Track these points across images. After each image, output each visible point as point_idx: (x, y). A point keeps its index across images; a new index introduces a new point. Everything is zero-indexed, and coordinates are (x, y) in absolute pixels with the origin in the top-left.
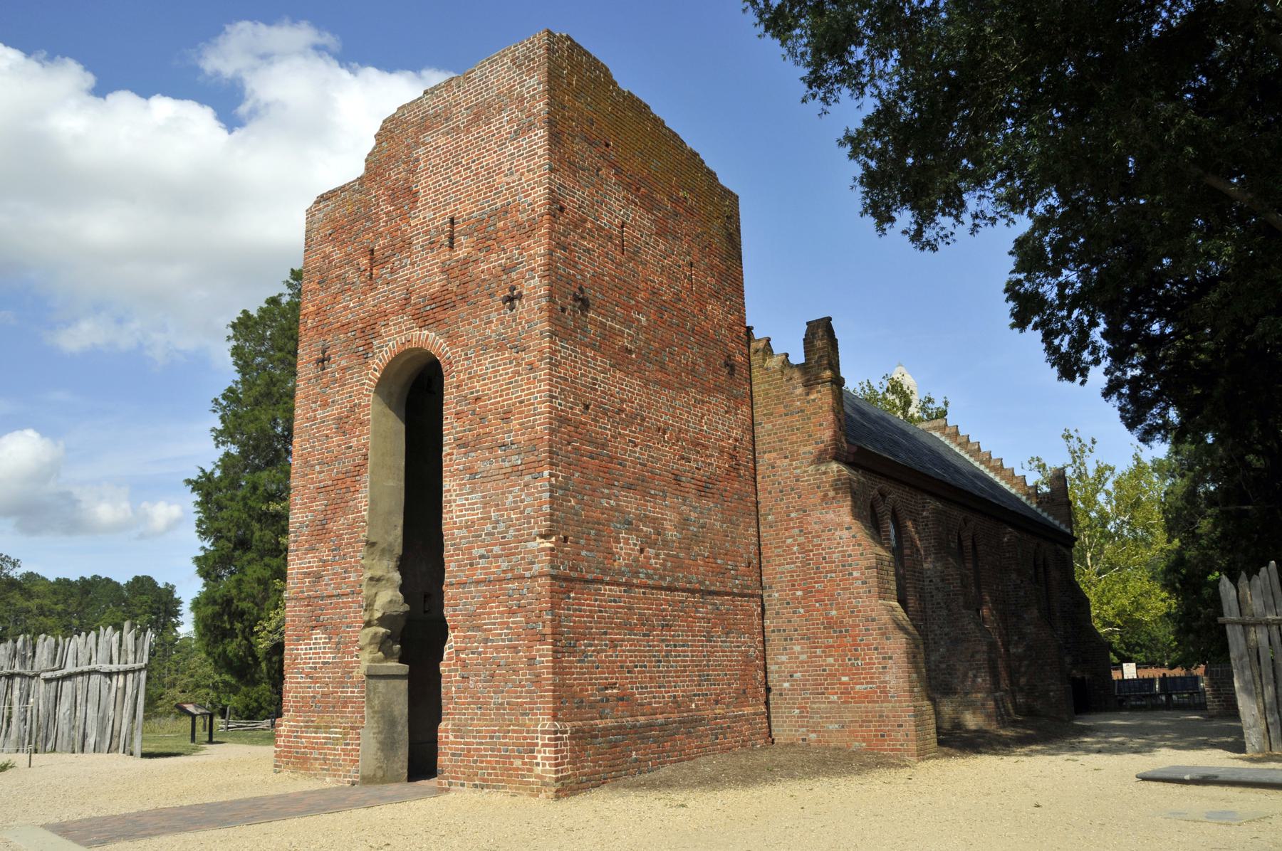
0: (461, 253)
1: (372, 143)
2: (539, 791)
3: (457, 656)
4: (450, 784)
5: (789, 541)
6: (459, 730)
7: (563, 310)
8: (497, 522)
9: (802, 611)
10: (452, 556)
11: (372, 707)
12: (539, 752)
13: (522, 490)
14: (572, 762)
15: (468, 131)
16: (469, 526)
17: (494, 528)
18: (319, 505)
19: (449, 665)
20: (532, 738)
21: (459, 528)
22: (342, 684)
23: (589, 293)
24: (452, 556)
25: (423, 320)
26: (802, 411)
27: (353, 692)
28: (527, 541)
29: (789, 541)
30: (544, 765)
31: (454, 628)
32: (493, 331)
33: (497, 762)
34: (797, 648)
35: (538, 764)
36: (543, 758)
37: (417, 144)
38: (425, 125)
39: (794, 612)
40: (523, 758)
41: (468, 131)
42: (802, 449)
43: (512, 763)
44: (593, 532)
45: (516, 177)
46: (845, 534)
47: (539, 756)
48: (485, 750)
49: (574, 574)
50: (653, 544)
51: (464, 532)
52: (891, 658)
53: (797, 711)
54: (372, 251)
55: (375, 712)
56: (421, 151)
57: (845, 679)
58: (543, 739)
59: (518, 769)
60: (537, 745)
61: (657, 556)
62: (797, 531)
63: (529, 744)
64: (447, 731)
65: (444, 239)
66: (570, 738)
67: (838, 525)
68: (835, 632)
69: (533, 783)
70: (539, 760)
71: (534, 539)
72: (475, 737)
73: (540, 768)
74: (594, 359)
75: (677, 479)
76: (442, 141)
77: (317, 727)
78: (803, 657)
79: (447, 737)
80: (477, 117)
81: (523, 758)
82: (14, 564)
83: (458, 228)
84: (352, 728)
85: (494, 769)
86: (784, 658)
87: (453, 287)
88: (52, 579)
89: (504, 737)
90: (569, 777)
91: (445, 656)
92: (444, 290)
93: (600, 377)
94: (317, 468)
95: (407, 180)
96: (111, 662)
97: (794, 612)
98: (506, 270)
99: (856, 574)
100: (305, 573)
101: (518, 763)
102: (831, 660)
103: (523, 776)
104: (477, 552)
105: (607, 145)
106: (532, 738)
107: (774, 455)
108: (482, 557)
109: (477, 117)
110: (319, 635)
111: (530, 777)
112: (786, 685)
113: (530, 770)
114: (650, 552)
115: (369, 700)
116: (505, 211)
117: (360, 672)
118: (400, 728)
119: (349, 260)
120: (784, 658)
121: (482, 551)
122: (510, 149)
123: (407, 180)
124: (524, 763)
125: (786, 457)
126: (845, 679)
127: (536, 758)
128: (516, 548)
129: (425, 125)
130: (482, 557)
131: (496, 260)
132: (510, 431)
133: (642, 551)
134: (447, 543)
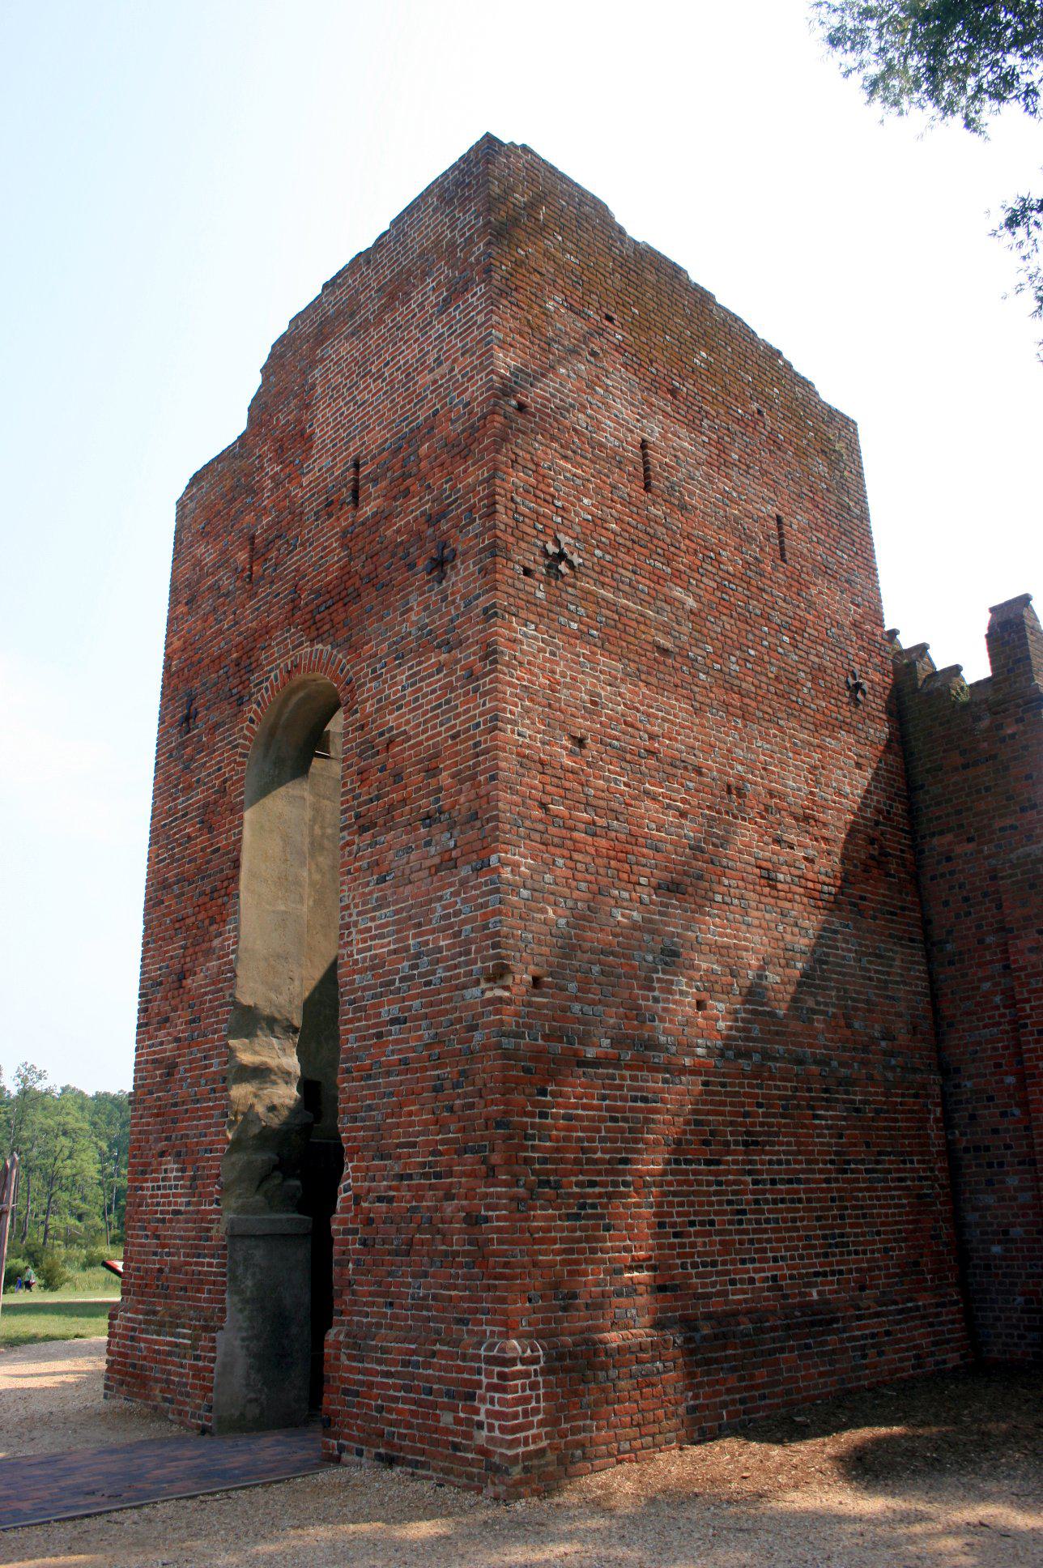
0: (368, 510)
1: (258, 380)
2: (483, 1479)
3: (357, 1204)
4: (342, 1448)
5: (986, 986)
6: (356, 1346)
8: (418, 956)
9: (1017, 1111)
10: (351, 1021)
11: (239, 1292)
12: (483, 1400)
13: (455, 894)
14: (551, 1421)
15: (381, 321)
16: (376, 965)
17: (414, 967)
19: (343, 1222)
20: (471, 1370)
21: (360, 972)
24: (351, 1021)
25: (315, 630)
26: (994, 757)
27: (209, 1265)
28: (465, 987)
30: (491, 1428)
31: (355, 1151)
32: (413, 624)
33: (414, 1414)
35: (480, 1425)
36: (489, 1413)
37: (313, 365)
39: (1003, 1114)
40: (455, 1410)
41: (381, 321)
43: (437, 1418)
44: (596, 969)
45: (445, 367)
47: (483, 1408)
48: (397, 1388)
51: (368, 979)
53: (1020, 1299)
54: (253, 537)
55: (245, 1301)
58: (489, 1375)
59: (447, 1431)
60: (479, 1384)
62: (998, 966)
63: (466, 1383)
64: (338, 1345)
65: (346, 493)
66: (544, 1372)
69: (471, 1463)
70: (482, 1417)
71: (477, 983)
72: (380, 1362)
73: (485, 1433)
75: (770, 880)
77: (161, 1324)
79: (337, 1358)
80: (392, 297)
81: (455, 1410)
82: (40, 1077)
83: (365, 471)
84: (205, 1329)
85: (409, 1426)
87: (357, 566)
88: (91, 1093)
89: (427, 1365)
90: (541, 1452)
91: (339, 1206)
92: (346, 572)
93: (605, 692)
95: (299, 421)
97: (1003, 1114)
98: (432, 520)
100: (154, 1061)
101: (447, 1419)
103: (456, 1447)
104: (388, 1011)
106: (471, 1370)
107: (950, 837)
108: (394, 1021)
109: (392, 297)
111: (467, 1449)
112: (996, 1249)
113: (468, 1436)
115: (234, 1279)
116: (430, 426)
117: (218, 1231)
118: (294, 1330)
119: (224, 561)
122: (438, 327)
123: (299, 421)
124: (458, 1421)
125: (970, 840)
127: (477, 1412)
128: (449, 1000)
131: (420, 505)
132: (440, 790)
133: (700, 1005)
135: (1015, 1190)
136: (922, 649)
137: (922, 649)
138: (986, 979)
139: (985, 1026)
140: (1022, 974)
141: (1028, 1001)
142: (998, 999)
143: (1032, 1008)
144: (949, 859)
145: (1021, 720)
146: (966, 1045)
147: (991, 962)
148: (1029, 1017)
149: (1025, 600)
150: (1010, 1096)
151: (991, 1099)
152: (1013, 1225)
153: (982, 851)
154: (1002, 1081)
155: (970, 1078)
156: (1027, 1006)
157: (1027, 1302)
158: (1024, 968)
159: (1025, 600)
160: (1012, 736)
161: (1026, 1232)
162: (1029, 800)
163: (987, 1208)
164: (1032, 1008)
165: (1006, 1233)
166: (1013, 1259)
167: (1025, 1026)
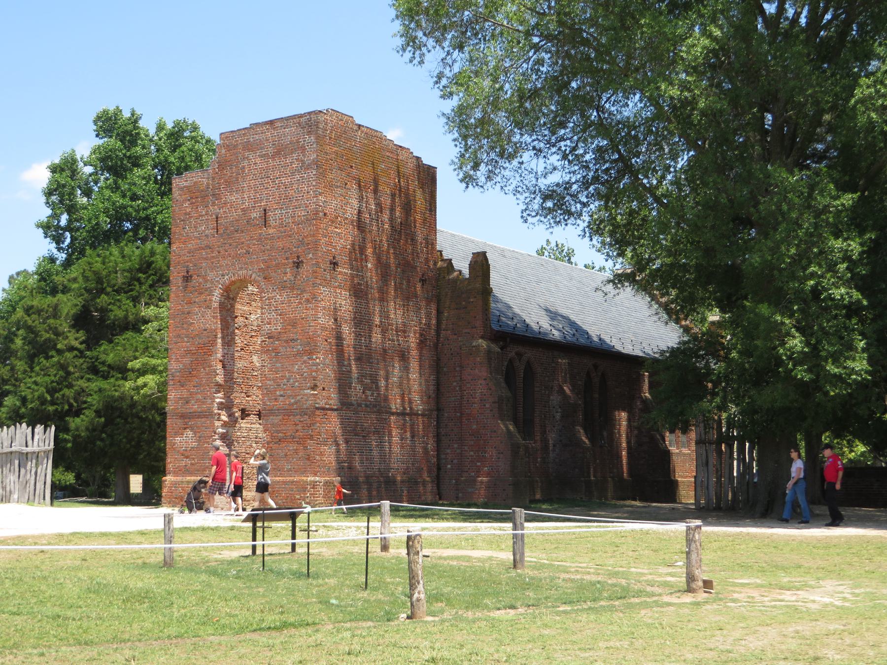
5: (455, 384)
7: (325, 270)
18: (187, 360)
22: (203, 459)
23: (338, 258)
34: (456, 446)
38: (249, 147)
46: (483, 382)
49: (327, 406)
50: (370, 389)
56: (246, 163)
57: (479, 464)
61: (372, 395)
74: (341, 294)
76: (258, 160)
86: (449, 451)
96: (27, 446)
99: (487, 406)
102: (472, 453)
105: (351, 167)
108: (281, 396)
110: (190, 433)
114: (369, 393)
120: (449, 451)
121: (282, 393)
126: (479, 464)
129: (249, 147)
130: (281, 396)
133: (363, 392)
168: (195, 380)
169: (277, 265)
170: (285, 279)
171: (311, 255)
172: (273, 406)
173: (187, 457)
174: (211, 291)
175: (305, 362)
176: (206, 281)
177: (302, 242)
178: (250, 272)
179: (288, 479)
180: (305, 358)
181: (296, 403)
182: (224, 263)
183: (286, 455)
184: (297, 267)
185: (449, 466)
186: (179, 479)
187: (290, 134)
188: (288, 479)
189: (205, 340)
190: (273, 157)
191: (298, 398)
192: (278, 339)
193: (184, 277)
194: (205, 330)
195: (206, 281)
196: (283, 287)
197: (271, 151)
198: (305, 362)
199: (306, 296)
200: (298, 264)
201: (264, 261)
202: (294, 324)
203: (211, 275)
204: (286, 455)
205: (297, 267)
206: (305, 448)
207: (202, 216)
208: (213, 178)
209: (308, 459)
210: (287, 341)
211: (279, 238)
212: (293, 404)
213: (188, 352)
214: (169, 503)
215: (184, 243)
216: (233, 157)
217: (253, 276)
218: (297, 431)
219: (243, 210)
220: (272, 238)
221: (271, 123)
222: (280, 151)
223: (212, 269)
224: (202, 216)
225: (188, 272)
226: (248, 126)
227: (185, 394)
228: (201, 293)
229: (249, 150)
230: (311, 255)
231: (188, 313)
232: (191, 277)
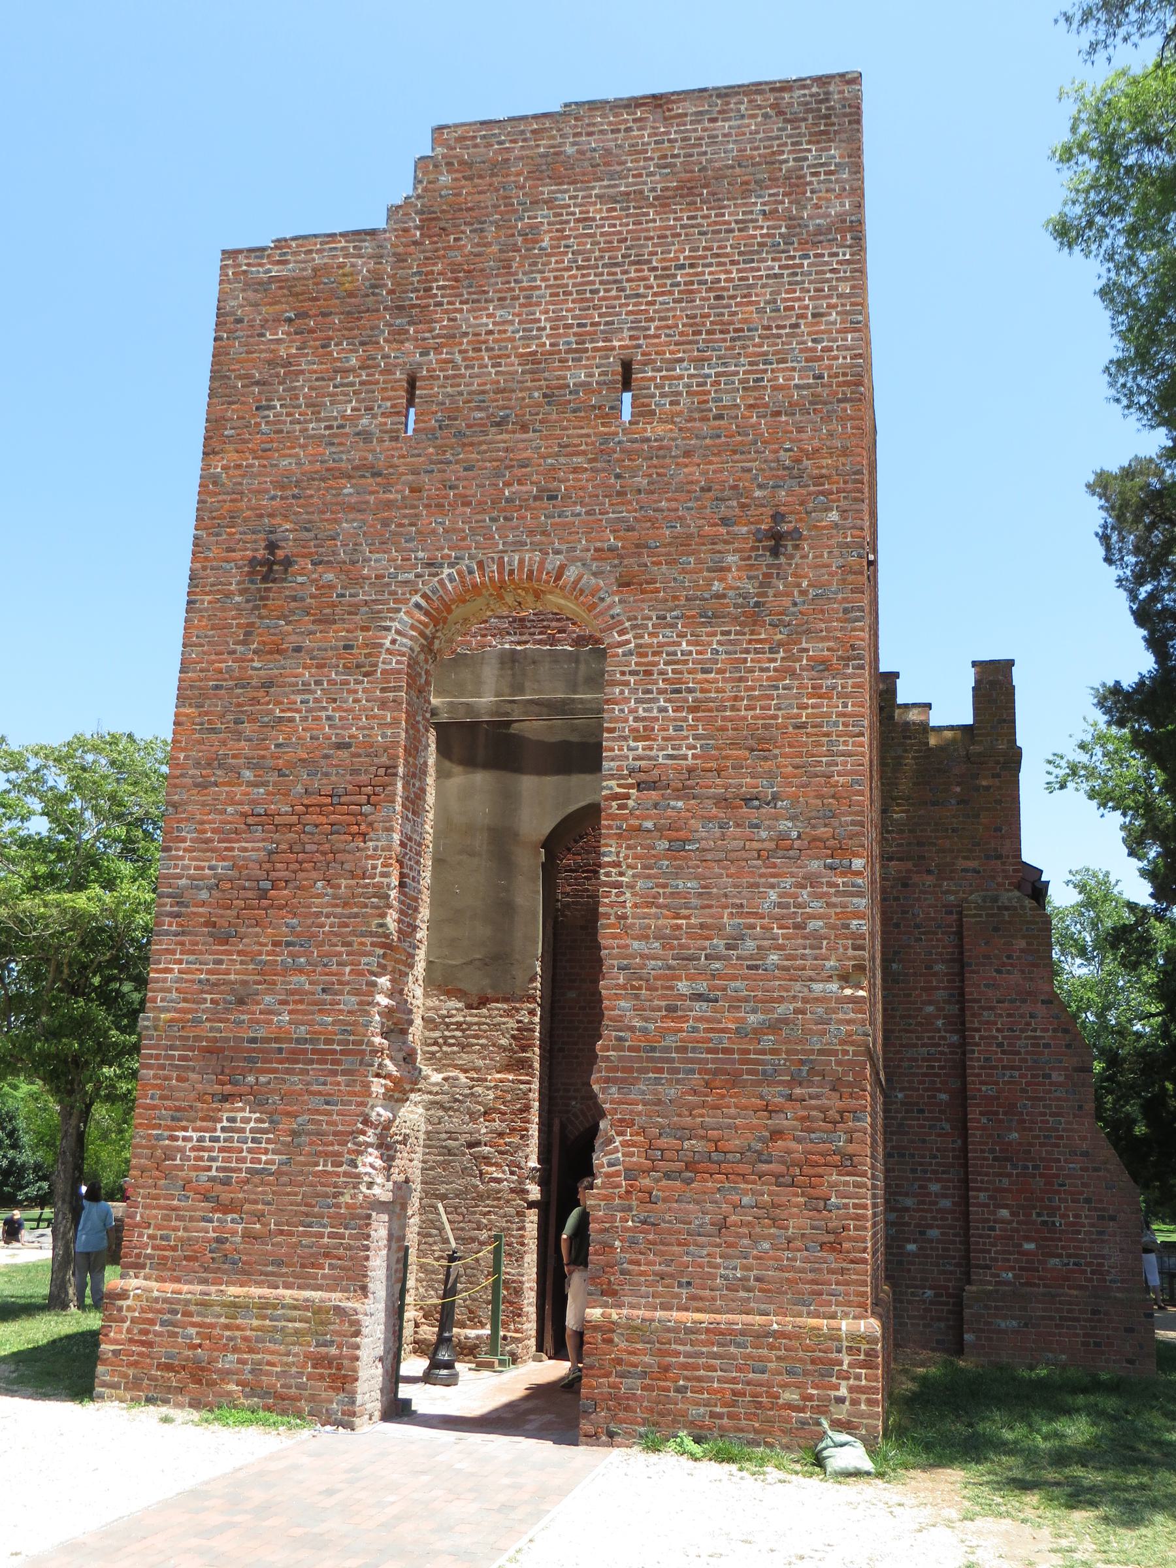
5: (930, 1009)
18: (252, 848)
29: (930, 1009)
30: (855, 1403)
34: (935, 1187)
35: (841, 1400)
36: (851, 1389)
38: (555, 169)
42: (961, 863)
52: (1112, 1218)
53: (929, 1293)
56: (543, 216)
57: (1030, 1246)
67: (1029, 993)
68: (1015, 1167)
70: (843, 1392)
76: (597, 211)
78: (946, 1203)
94: (248, 774)
99: (1056, 1077)
102: (1004, 1213)
108: (699, 997)
110: (247, 1117)
121: (702, 987)
125: (929, 872)
126: (1030, 1246)
129: (555, 169)
130: (699, 997)
134: (611, 961)
135: (936, 1195)
136: (1117, 683)
137: (1117, 683)
138: (930, 1003)
139: (923, 1045)
140: (976, 1005)
141: (978, 1030)
142: (940, 1023)
143: (981, 1038)
144: (905, 885)
145: (998, 776)
146: (901, 1060)
147: (937, 988)
148: (978, 1045)
149: (1011, 663)
150: (940, 1112)
151: (921, 1111)
152: (931, 1227)
153: (940, 886)
154: (934, 1097)
155: (902, 1090)
156: (977, 1035)
157: (936, 1295)
158: (979, 1001)
159: (1011, 663)
160: (987, 788)
161: (942, 1234)
162: (996, 850)
163: (907, 1209)
164: (981, 1038)
165: (922, 1233)
166: (926, 1256)
167: (973, 1052)
168: (285, 925)
169: (684, 543)
170: (717, 586)
171: (834, 516)
172: (663, 1032)
173: (226, 1208)
174: (376, 616)
175: (811, 880)
176: (357, 581)
177: (794, 471)
178: (558, 560)
179: (740, 1320)
180: (815, 865)
181: (774, 1027)
182: (436, 523)
183: (722, 1226)
184: (775, 552)
185: (912, 1247)
186: (190, 1290)
187: (730, 140)
188: (740, 1320)
189: (344, 782)
190: (663, 203)
191: (782, 1009)
192: (683, 792)
193: (253, 562)
194: (340, 746)
195: (357, 581)
196: (707, 613)
197: (653, 183)
198: (811, 880)
199: (815, 648)
200: (776, 541)
201: (621, 527)
202: (761, 744)
203: (376, 563)
204: (722, 1226)
205: (775, 552)
206: (818, 1204)
207: (346, 371)
208: (400, 259)
209: (834, 1247)
210: (722, 801)
211: (687, 454)
212: (758, 1032)
213: (257, 819)
214: (134, 1384)
215: (264, 452)
216: (489, 199)
217: (571, 573)
218: (776, 1134)
219: (531, 359)
220: (660, 451)
221: (658, 102)
222: (692, 187)
223: (382, 546)
224: (346, 371)
225: (272, 547)
226: (556, 108)
227: (235, 969)
228: (327, 621)
229: (558, 180)
230: (834, 516)
231: (267, 685)
232: (287, 562)
